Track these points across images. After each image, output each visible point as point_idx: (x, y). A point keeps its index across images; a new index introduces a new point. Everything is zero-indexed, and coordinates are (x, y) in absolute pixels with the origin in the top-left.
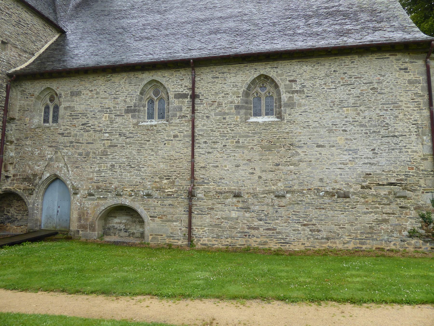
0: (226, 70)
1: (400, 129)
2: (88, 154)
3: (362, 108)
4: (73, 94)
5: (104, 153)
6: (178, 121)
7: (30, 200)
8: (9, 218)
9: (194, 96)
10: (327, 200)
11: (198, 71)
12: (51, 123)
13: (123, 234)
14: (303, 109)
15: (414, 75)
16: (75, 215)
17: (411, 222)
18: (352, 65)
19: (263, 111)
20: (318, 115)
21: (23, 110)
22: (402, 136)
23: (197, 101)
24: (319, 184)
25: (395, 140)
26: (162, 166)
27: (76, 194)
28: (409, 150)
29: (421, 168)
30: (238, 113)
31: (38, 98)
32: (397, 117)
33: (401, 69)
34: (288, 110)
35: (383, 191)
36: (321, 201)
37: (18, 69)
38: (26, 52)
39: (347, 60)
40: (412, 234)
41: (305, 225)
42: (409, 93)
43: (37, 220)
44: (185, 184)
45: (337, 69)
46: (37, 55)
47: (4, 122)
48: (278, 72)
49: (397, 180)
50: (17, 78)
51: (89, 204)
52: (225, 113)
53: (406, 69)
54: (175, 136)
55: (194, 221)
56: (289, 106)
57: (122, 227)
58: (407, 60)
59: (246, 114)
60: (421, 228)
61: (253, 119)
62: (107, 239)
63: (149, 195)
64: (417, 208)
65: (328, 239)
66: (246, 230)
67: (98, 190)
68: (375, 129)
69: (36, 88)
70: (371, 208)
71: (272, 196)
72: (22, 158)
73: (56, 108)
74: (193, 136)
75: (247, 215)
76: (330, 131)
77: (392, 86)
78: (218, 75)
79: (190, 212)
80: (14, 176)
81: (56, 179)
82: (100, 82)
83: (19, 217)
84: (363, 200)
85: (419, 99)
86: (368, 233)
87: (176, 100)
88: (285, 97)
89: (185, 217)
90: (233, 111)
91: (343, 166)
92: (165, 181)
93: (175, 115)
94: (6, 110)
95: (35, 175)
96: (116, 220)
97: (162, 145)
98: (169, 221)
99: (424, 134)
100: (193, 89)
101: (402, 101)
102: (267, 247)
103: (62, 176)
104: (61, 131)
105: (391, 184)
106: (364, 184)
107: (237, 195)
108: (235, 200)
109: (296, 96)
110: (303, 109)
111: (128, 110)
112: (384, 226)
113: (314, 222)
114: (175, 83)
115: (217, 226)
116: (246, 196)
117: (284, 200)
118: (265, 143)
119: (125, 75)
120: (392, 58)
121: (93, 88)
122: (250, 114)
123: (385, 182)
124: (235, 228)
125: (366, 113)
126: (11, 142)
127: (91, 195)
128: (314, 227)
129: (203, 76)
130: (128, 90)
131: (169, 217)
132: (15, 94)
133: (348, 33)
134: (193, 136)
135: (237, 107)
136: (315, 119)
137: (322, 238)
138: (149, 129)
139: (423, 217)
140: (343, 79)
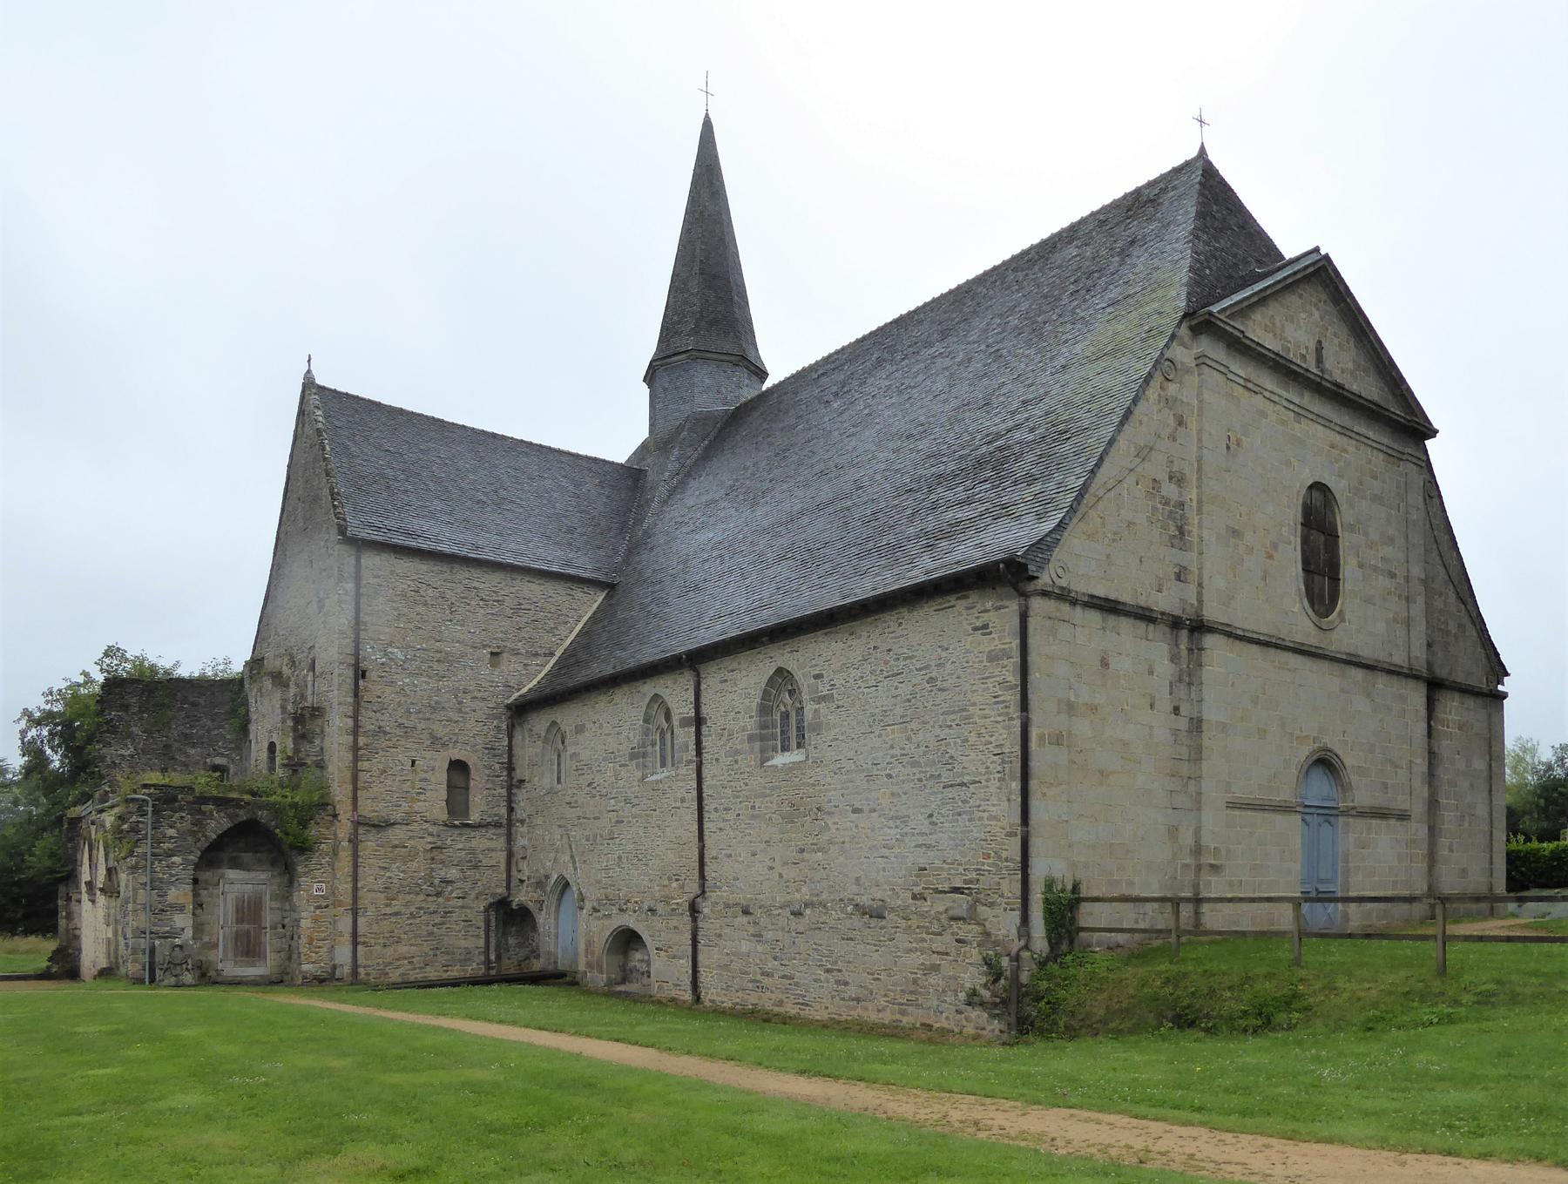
0: (735, 665)
3: (914, 725)
4: (580, 729)
7: (541, 918)
10: (857, 921)
15: (1000, 638)
18: (900, 631)
19: (794, 744)
22: (975, 782)
23: (704, 730)
24: (854, 889)
26: (670, 855)
28: (985, 815)
29: (1004, 854)
33: (975, 629)
37: (531, 685)
38: (536, 655)
39: (890, 618)
41: (828, 971)
43: (549, 953)
46: (558, 654)
47: (510, 788)
49: (965, 882)
50: (521, 710)
51: (595, 925)
52: (737, 752)
53: (985, 626)
55: (701, 958)
58: (989, 605)
59: (762, 751)
61: (780, 760)
62: (621, 988)
65: (858, 1000)
66: (759, 977)
75: (759, 948)
77: (959, 672)
78: (729, 676)
82: (602, 705)
84: (903, 924)
86: (912, 992)
88: (809, 709)
91: (886, 852)
92: (674, 885)
94: (511, 768)
99: (1013, 779)
101: (974, 704)
104: (568, 799)
105: (956, 890)
106: (917, 890)
107: (746, 912)
108: (745, 919)
111: (633, 756)
112: (933, 979)
113: (840, 965)
114: (676, 693)
115: (726, 967)
120: (961, 605)
122: (774, 749)
123: (946, 887)
124: (747, 973)
125: (920, 737)
126: (522, 822)
127: (595, 910)
133: (952, 531)
136: (851, 754)
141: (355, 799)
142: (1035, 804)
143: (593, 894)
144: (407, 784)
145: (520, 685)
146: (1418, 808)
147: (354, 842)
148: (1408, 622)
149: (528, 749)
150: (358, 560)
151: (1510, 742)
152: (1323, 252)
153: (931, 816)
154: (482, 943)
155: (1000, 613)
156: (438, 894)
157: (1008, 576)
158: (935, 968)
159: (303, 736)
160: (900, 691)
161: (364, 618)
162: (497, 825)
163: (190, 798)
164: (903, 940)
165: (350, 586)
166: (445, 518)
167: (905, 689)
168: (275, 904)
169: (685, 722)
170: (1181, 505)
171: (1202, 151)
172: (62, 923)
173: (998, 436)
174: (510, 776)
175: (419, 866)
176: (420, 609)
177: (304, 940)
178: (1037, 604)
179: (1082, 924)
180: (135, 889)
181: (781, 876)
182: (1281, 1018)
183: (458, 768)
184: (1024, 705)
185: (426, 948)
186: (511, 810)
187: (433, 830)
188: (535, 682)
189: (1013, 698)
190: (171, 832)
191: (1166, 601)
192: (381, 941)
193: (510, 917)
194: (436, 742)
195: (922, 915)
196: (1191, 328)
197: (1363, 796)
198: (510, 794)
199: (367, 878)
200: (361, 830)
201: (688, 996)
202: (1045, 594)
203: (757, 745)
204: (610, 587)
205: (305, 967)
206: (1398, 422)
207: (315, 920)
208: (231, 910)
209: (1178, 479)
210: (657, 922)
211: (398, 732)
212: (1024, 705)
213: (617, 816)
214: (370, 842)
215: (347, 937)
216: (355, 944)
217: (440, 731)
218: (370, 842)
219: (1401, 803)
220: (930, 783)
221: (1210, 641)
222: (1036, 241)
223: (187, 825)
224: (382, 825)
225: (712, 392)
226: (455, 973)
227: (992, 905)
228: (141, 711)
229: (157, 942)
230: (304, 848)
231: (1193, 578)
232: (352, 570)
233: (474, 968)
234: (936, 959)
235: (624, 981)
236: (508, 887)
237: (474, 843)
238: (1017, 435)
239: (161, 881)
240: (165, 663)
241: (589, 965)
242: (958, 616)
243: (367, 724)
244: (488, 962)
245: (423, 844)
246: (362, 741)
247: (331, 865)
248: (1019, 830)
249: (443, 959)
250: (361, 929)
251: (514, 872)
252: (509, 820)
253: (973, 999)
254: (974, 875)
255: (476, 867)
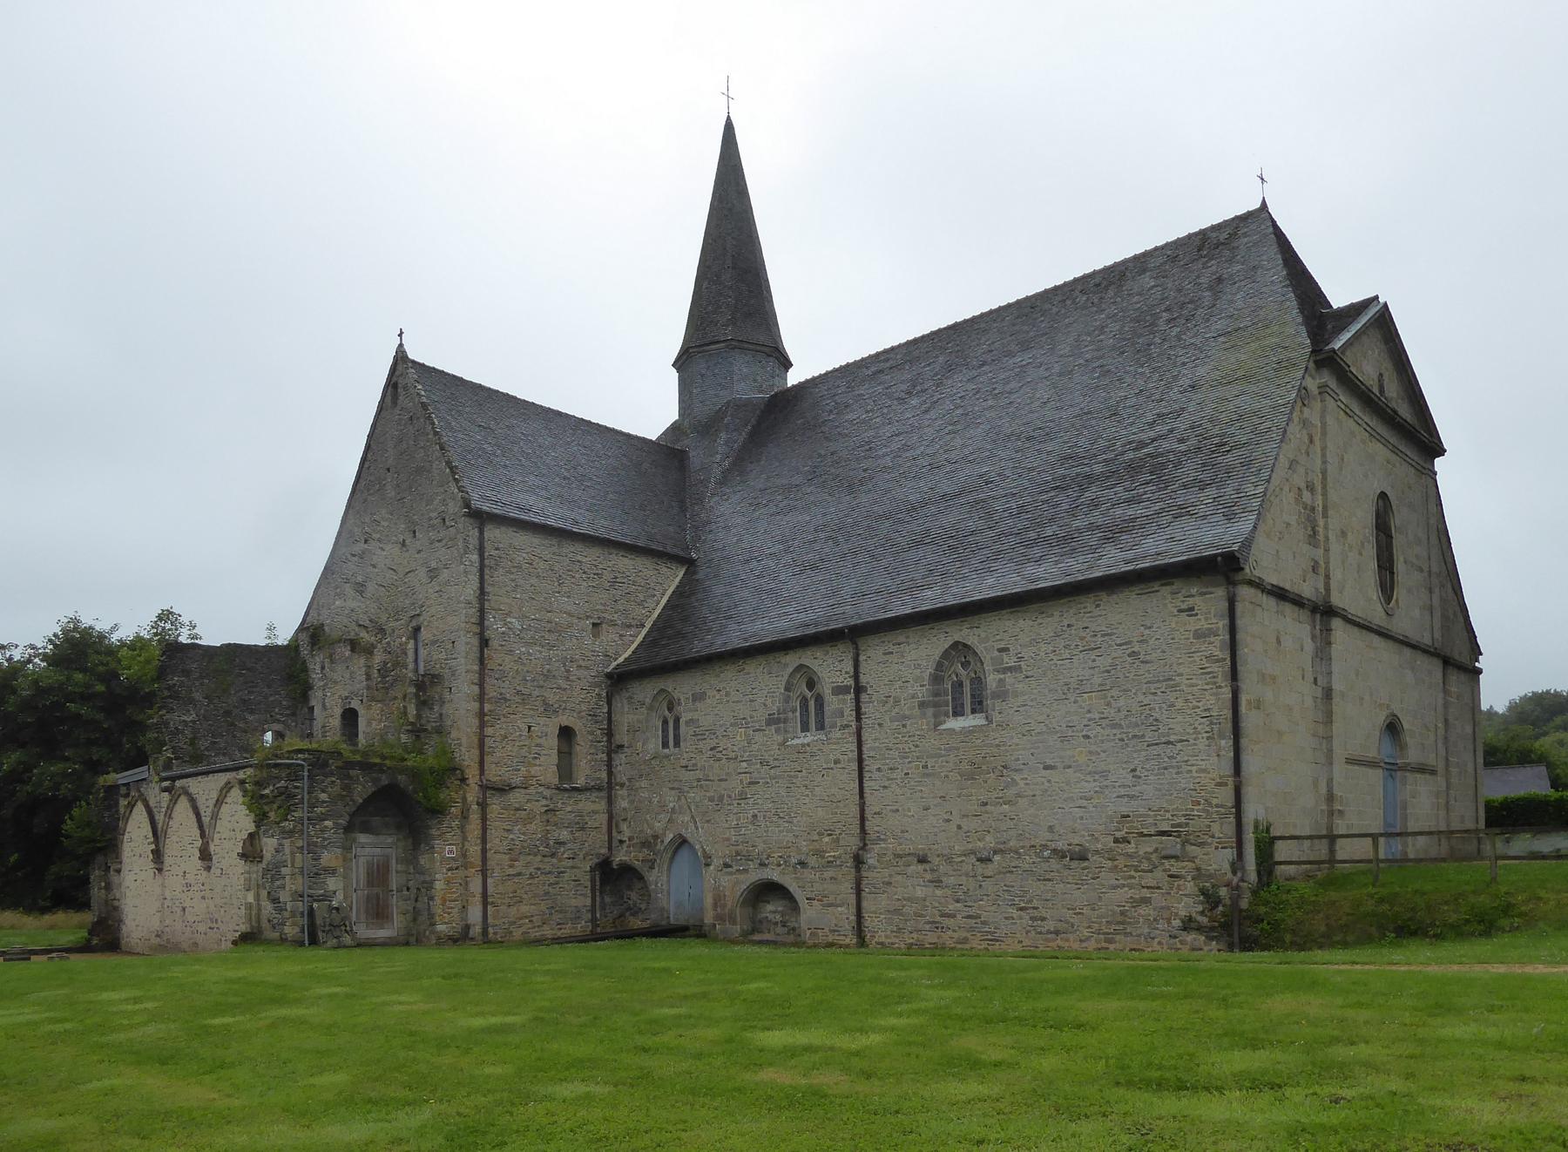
0: (901, 639)
1: (1178, 728)
2: (721, 798)
3: (1114, 692)
4: (698, 697)
5: (743, 797)
6: (838, 735)
8: (629, 909)
9: (859, 690)
10: (1054, 864)
11: (862, 642)
12: (672, 749)
13: (779, 929)
14: (1020, 700)
16: (709, 901)
17: (1187, 904)
18: (1097, 612)
20: (1044, 709)
21: (633, 731)
23: (864, 697)
24: (1048, 836)
25: (1169, 750)
26: (820, 812)
27: (708, 865)
29: (1215, 801)
30: (924, 715)
31: (651, 708)
32: (1173, 705)
33: (1180, 611)
34: (998, 704)
35: (1147, 847)
36: (1045, 866)
37: (626, 655)
38: (630, 626)
39: (1088, 602)
40: (1188, 925)
41: (1021, 909)
42: (1197, 657)
44: (852, 842)
45: (1073, 621)
46: (648, 625)
48: (983, 636)
50: (619, 680)
51: (726, 881)
52: (905, 717)
53: (1192, 609)
54: (836, 762)
55: (865, 904)
56: (999, 697)
57: (778, 918)
58: (1194, 591)
59: (935, 716)
60: (1202, 913)
62: (757, 937)
63: (802, 864)
64: (1199, 874)
65: (1057, 933)
67: (738, 858)
68: (1136, 731)
69: (645, 691)
70: (1124, 878)
71: (973, 859)
72: (638, 810)
73: (677, 721)
74: (860, 761)
75: (938, 892)
76: (1064, 739)
78: (892, 648)
79: (858, 891)
80: (630, 839)
81: (681, 843)
83: (643, 906)
85: (1215, 668)
87: (835, 698)
88: (992, 680)
89: (852, 899)
90: (916, 711)
91: (1085, 803)
92: (826, 839)
93: (834, 726)
94: (610, 734)
95: (656, 837)
96: (770, 907)
97: (820, 779)
98: (830, 905)
99: (1221, 736)
100: (856, 676)
102: (967, 946)
103: (688, 836)
104: (684, 763)
105: (1163, 833)
106: (1119, 835)
107: (922, 860)
108: (920, 867)
109: (1009, 678)
110: (1020, 700)
111: (771, 721)
112: (1143, 910)
113: (1035, 903)
114: (831, 667)
115: (897, 911)
116: (936, 861)
117: (990, 866)
118: (965, 767)
119: (761, 659)
120: (1166, 590)
121: (721, 686)
123: (1152, 830)
124: (921, 916)
125: (1122, 702)
126: (622, 785)
127: (727, 865)
128: (1036, 913)
129: (871, 653)
130: (765, 685)
131: (831, 898)
132: (620, 704)
134: (860, 761)
135: (922, 705)
136: (1041, 718)
137: (1049, 932)
138: (801, 749)
139: (1203, 892)
140: (1082, 639)
141: (482, 763)
142: (1246, 758)
143: (719, 853)
144: (523, 750)
145: (618, 655)
146: (1441, 768)
147: (483, 805)
148: (1431, 610)
149: (626, 717)
150: (481, 532)
151: (1484, 707)
152: (1381, 300)
153: (1134, 770)
154: (588, 902)
155: (1209, 602)
156: (553, 855)
157: (1223, 568)
158: (1146, 901)
159: (424, 703)
160: (1097, 663)
161: (488, 589)
162: (599, 789)
163: (340, 763)
164: (1108, 878)
165: (475, 557)
166: (543, 493)
167: (1104, 662)
168: (400, 867)
169: (840, 690)
170: (1313, 509)
171: (1264, 203)
172: (97, 893)
173: (1142, 445)
174: (609, 741)
175: (536, 827)
176: (534, 581)
177: (438, 901)
178: (1245, 592)
179: (1278, 858)
180: (293, 854)
181: (959, 827)
182: (1504, 922)
183: (566, 733)
184: (1234, 674)
185: (543, 907)
186: (610, 773)
187: (547, 793)
188: (629, 652)
189: (1221, 671)
190: (324, 796)
191: (1307, 590)
192: (507, 901)
193: (614, 877)
194: (549, 710)
195: (1130, 856)
196: (1316, 362)
197: (1413, 756)
198: (610, 760)
199: (494, 842)
200: (488, 793)
201: (851, 939)
202: (1251, 583)
203: (930, 711)
204: (690, 563)
205: (440, 928)
206: (1432, 447)
207: (448, 882)
208: (362, 871)
209: (1311, 488)
210: (807, 874)
211: (517, 699)
212: (1234, 674)
213: (746, 779)
214: (495, 806)
215: (478, 898)
216: (485, 904)
217: (552, 698)
218: (495, 806)
219: (1431, 760)
220: (1133, 742)
221: (1336, 623)
222: (1099, 267)
223: (337, 789)
224: (503, 789)
225: (745, 383)
226: (567, 931)
227: (1201, 845)
228: (201, 677)
229: (315, 905)
230: (438, 811)
231: (1322, 571)
232: (476, 542)
233: (583, 926)
234: (1146, 893)
235: (754, 931)
236: (610, 848)
237: (581, 805)
238: (1166, 445)
239: (315, 844)
240: (101, 626)
241: (720, 918)
242: (1163, 605)
243: (491, 693)
244: (593, 920)
245: (539, 807)
246: (487, 707)
247: (462, 828)
248: (1231, 781)
249: (557, 917)
250: (490, 890)
251: (614, 834)
252: (609, 782)
253: (1188, 925)
254: (1183, 820)
255: (583, 829)
